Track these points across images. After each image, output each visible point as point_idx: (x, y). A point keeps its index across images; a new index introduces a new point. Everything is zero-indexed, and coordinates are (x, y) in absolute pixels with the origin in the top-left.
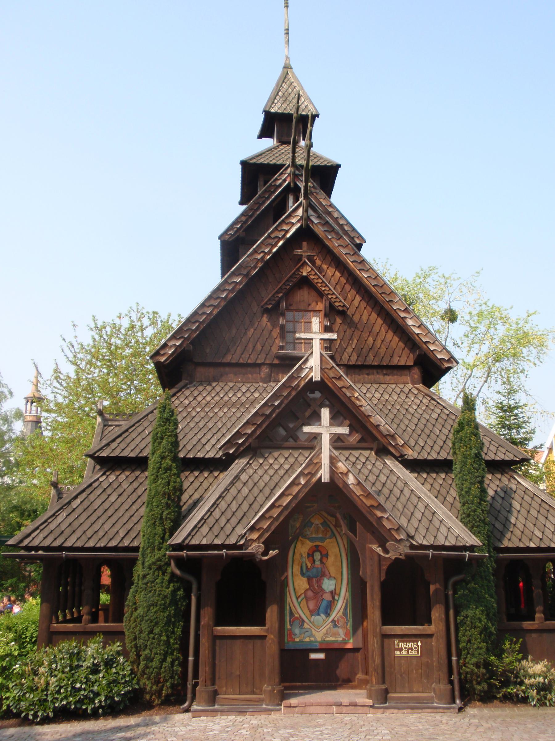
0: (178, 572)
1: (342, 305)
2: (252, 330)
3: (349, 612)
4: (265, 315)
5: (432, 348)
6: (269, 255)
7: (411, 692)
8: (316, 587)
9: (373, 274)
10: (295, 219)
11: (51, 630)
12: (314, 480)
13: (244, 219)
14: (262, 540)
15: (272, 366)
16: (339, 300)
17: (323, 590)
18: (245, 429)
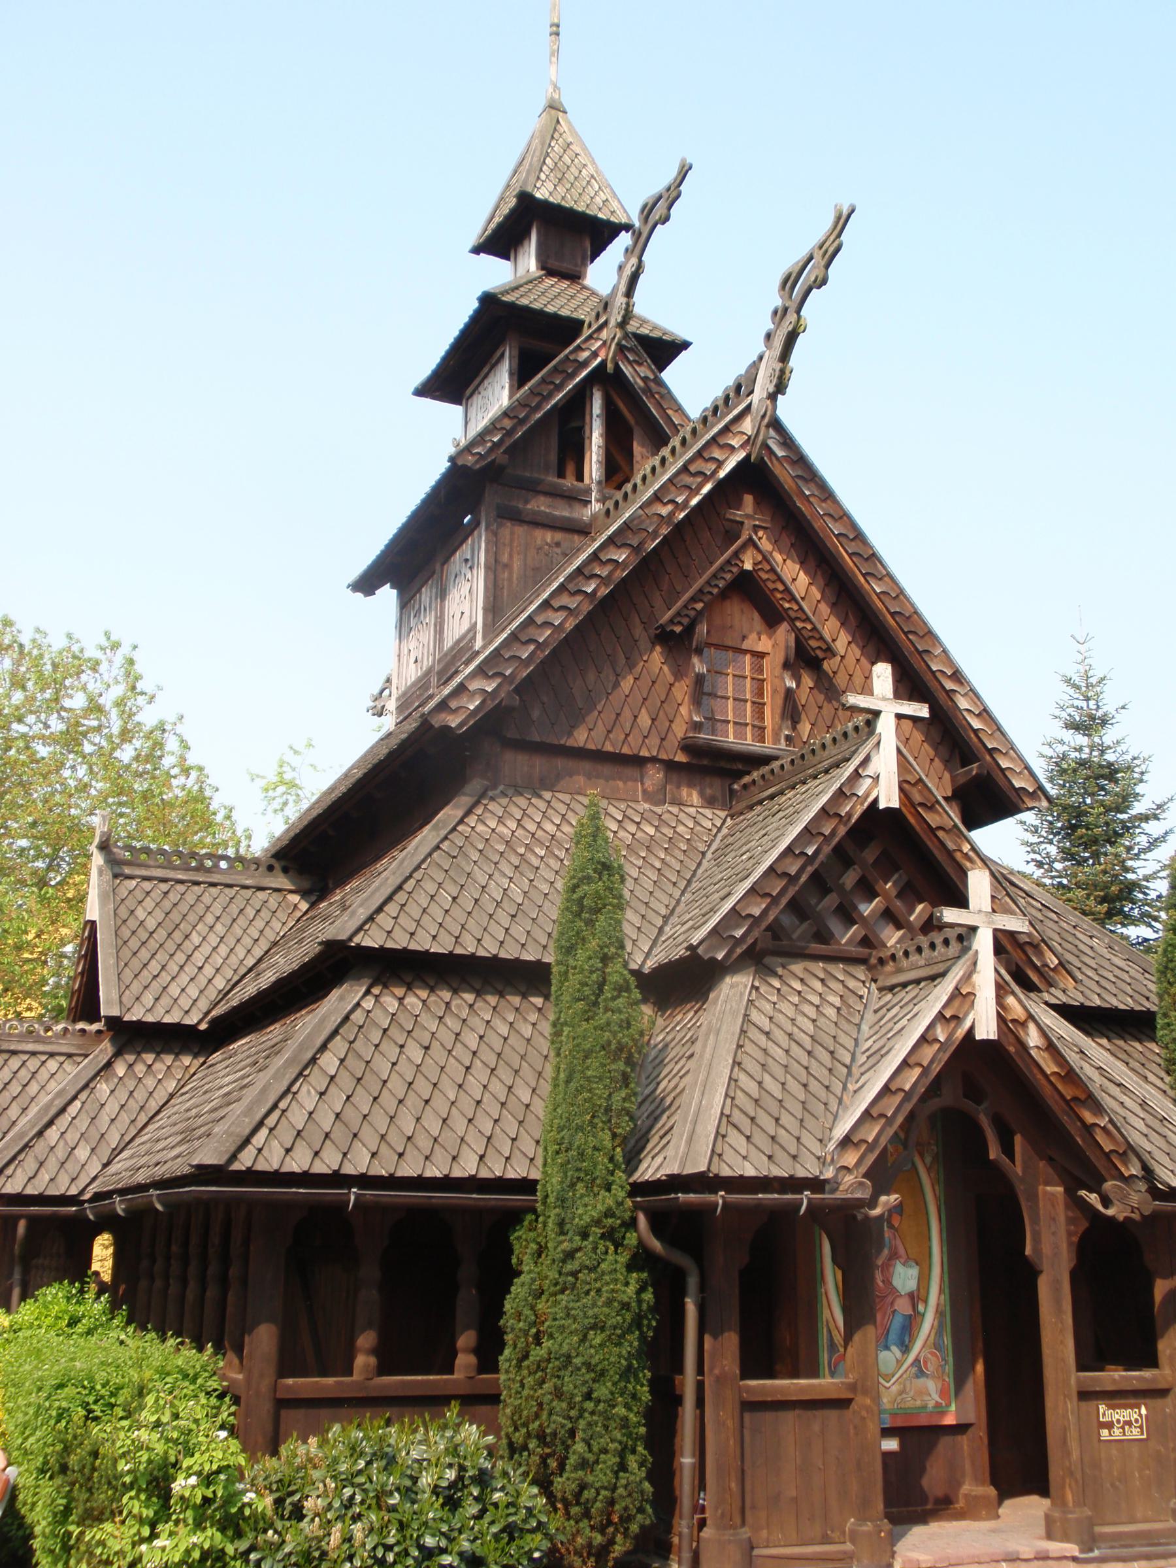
0: (656, 1245)
1: (824, 647)
2: (630, 679)
3: (947, 1341)
4: (658, 649)
5: (1004, 763)
6: (682, 510)
7: (1133, 1521)
8: (881, 1284)
9: (893, 589)
10: (737, 439)
11: (279, 1396)
12: (961, 1033)
13: (508, 423)
14: (863, 1169)
15: (670, 766)
16: (817, 636)
17: (894, 1290)
18: (748, 905)
